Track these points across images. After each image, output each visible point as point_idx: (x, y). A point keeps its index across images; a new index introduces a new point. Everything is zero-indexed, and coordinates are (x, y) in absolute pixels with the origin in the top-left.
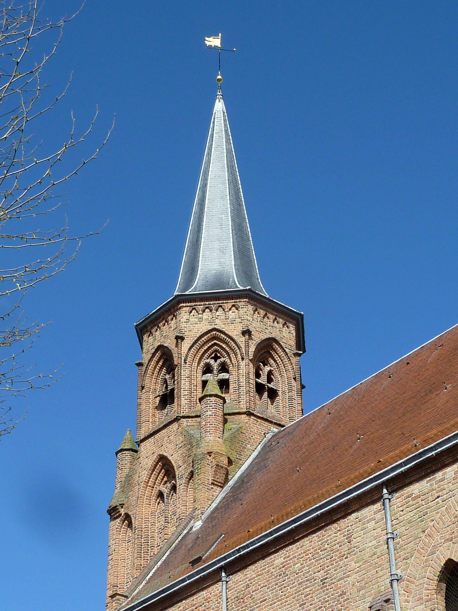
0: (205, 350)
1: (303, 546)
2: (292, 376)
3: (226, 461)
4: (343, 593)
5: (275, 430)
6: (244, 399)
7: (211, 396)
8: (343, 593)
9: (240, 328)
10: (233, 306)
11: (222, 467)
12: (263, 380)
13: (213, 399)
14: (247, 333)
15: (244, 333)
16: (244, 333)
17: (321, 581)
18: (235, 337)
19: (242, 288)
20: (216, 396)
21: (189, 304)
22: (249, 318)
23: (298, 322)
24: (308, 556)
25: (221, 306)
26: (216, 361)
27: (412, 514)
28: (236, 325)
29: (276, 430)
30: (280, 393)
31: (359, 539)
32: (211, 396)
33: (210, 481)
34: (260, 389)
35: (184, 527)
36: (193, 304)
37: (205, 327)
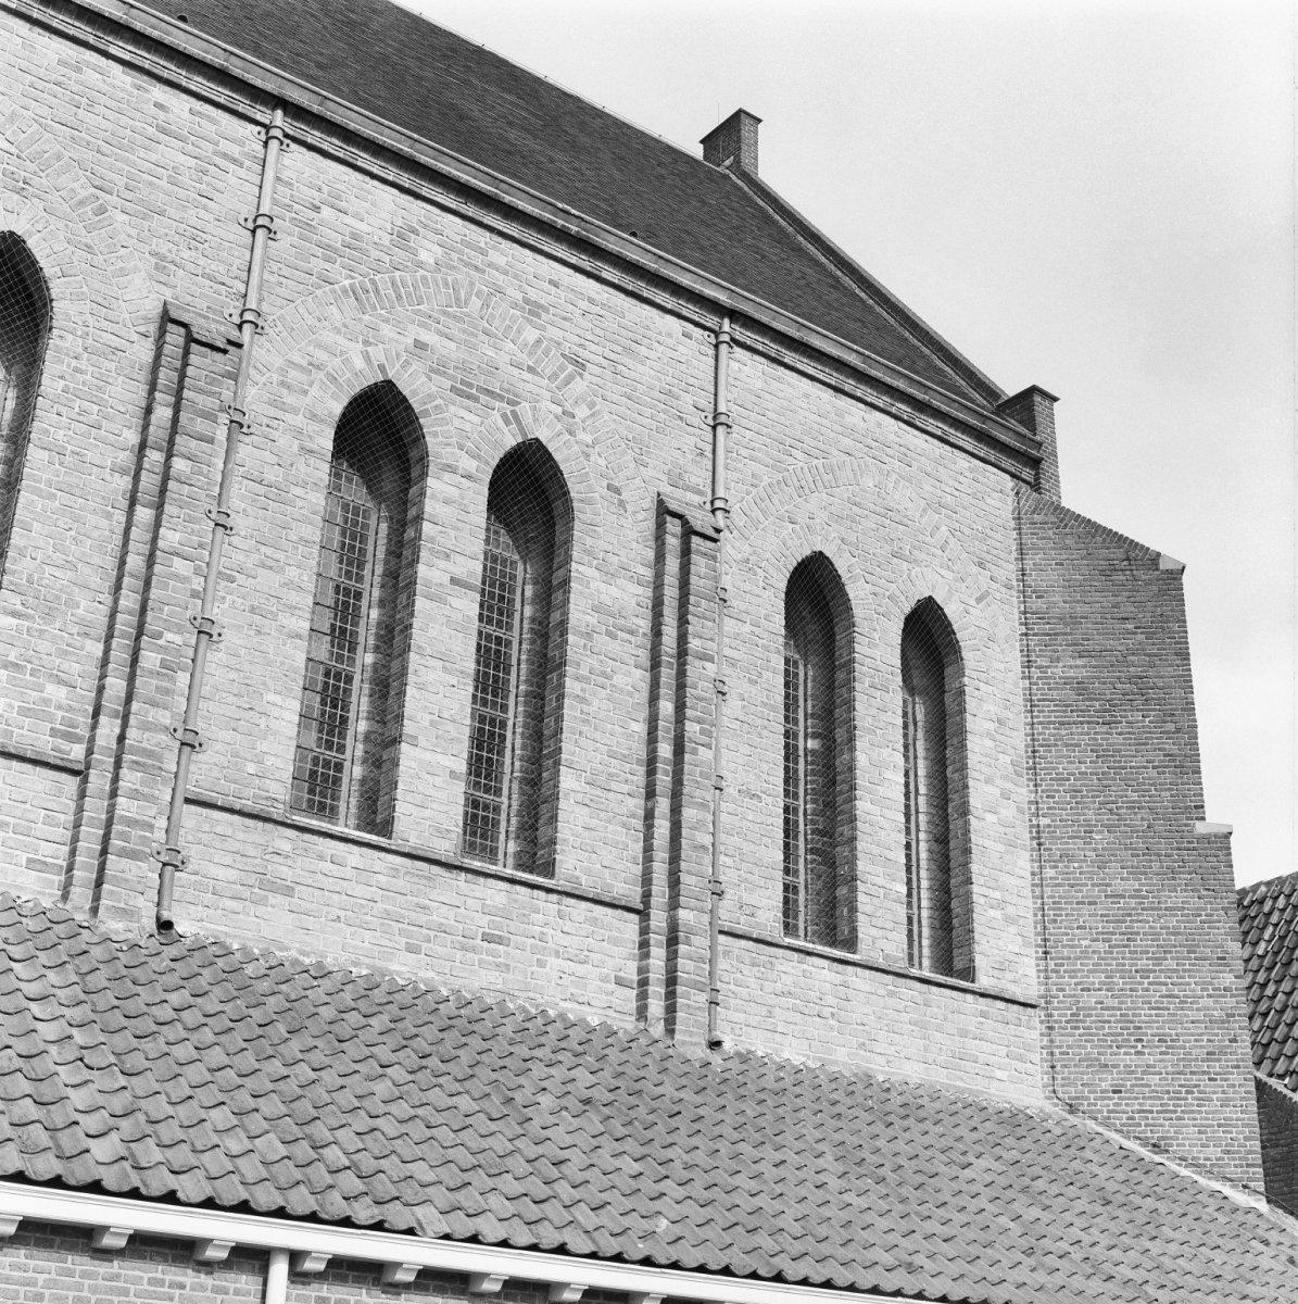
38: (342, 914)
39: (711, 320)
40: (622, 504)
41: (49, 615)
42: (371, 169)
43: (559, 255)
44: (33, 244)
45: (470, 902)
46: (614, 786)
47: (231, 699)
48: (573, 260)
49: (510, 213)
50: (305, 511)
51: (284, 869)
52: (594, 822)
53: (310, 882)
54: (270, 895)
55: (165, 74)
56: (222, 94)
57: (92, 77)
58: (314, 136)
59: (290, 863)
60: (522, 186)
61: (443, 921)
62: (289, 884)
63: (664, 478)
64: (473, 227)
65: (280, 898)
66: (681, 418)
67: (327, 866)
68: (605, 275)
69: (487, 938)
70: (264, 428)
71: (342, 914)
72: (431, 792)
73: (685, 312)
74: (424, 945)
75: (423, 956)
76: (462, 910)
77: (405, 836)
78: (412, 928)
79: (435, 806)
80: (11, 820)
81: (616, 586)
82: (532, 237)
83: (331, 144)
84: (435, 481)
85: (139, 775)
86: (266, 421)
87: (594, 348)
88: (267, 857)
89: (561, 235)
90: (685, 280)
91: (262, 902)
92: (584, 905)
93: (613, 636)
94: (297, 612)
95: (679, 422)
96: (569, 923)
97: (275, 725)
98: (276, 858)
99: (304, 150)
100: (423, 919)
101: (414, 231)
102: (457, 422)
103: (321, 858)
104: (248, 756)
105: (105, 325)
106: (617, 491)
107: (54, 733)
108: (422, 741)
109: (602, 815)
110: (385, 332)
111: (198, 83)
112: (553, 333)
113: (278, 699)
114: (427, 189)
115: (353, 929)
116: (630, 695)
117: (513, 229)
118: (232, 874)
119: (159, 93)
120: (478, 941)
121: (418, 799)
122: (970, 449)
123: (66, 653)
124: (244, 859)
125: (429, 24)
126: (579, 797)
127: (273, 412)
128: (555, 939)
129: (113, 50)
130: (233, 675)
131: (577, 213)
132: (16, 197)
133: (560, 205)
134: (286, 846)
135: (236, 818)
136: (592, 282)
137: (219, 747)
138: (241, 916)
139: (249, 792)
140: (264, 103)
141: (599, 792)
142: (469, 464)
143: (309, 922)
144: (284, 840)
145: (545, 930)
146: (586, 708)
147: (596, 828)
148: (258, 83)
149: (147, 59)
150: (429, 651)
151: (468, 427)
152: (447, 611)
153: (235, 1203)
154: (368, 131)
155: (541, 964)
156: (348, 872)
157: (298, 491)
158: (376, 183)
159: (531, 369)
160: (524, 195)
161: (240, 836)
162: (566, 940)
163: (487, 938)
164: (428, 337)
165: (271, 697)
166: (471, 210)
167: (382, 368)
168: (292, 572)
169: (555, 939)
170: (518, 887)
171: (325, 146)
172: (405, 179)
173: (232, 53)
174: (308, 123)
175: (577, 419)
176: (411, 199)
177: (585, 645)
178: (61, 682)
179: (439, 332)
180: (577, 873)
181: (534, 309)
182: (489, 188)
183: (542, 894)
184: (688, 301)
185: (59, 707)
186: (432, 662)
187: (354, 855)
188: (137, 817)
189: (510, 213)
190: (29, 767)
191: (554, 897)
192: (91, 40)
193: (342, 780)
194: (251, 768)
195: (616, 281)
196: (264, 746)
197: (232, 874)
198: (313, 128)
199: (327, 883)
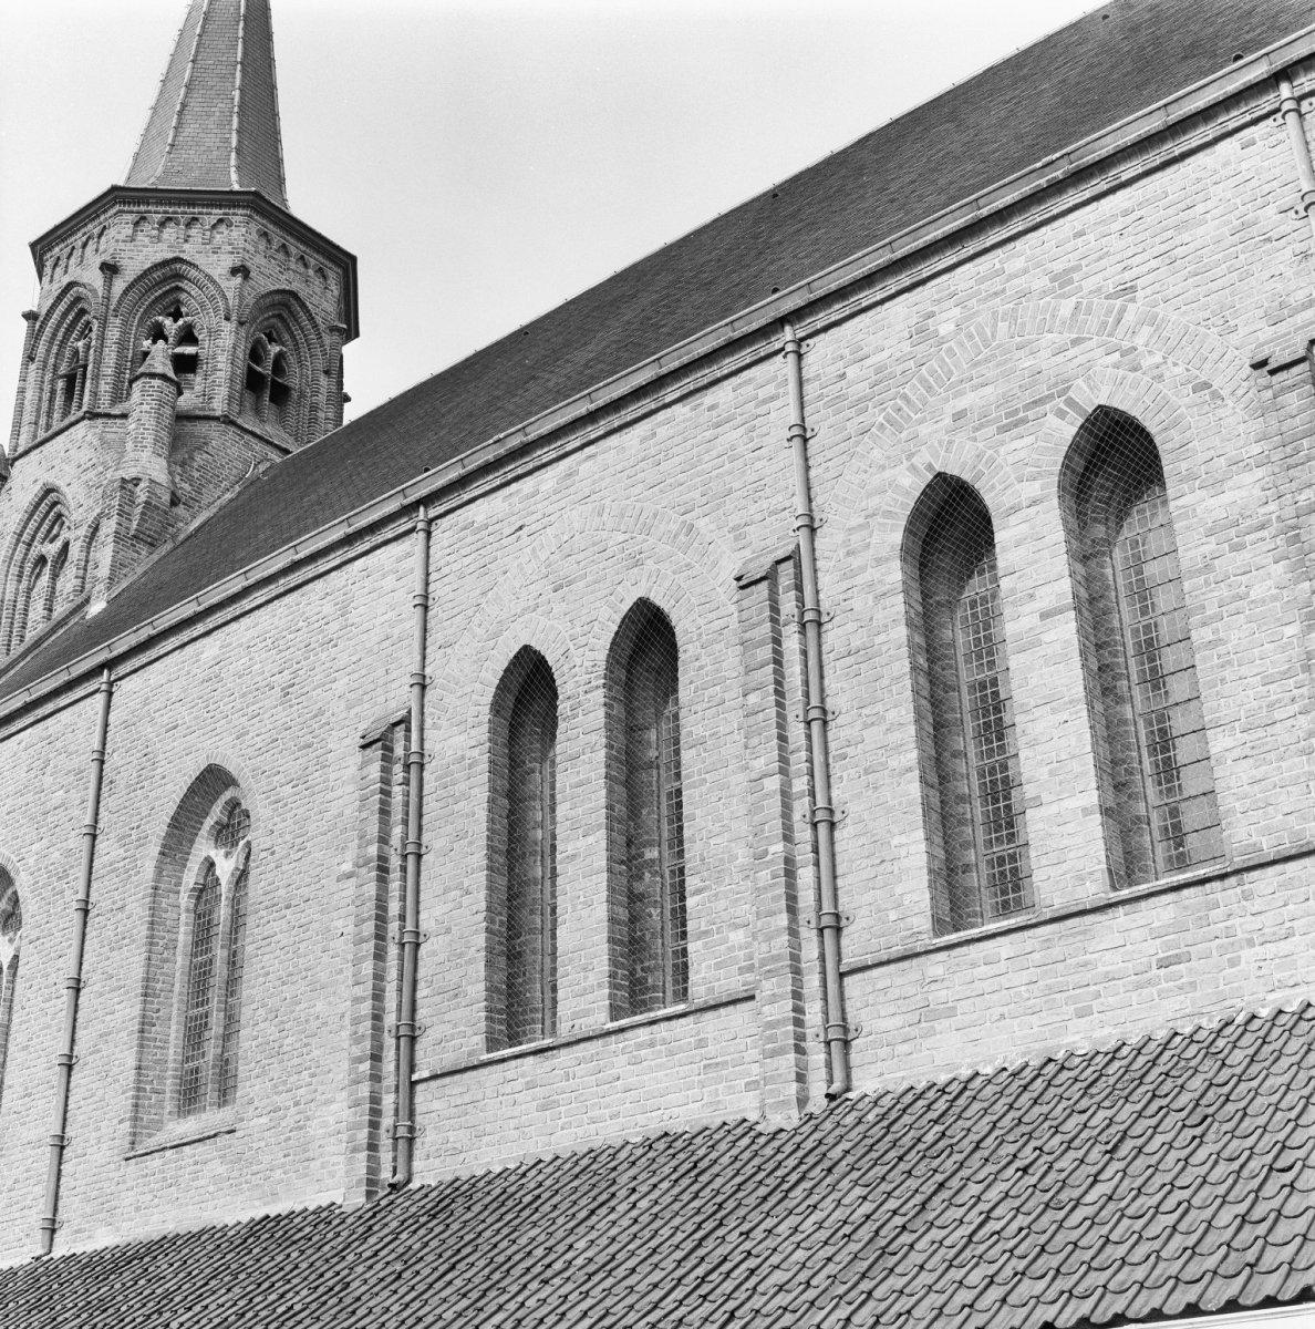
0: (156, 298)
1: (257, 624)
2: (320, 367)
3: (166, 498)
4: (321, 712)
5: (277, 458)
6: (222, 393)
7: (153, 376)
8: (321, 712)
9: (229, 261)
10: (221, 221)
11: (158, 508)
12: (266, 369)
13: (156, 382)
14: (241, 271)
15: (234, 271)
16: (234, 271)
17: (282, 690)
18: (216, 278)
19: (236, 187)
20: (163, 377)
21: (136, 209)
22: (249, 247)
23: (346, 271)
24: (264, 644)
25: (197, 219)
26: (175, 321)
27: (467, 561)
28: (223, 257)
29: (278, 460)
30: (295, 395)
31: (362, 610)
32: (153, 376)
33: (132, 532)
34: (253, 382)
35: (382, 791)
36: (142, 208)
37: (162, 253)
38: (1005, 1010)
39: (1266, 103)
40: (1216, 396)
41: (719, 881)
42: (874, 300)
43: (1070, 204)
44: (1116, 404)
45: (1134, 934)
46: (1277, 715)
47: (865, 862)
48: (1087, 195)
49: (1001, 216)
50: (892, 652)
51: (944, 992)
52: (1258, 774)
53: (968, 994)
54: (936, 1024)
55: (705, 381)
56: (745, 356)
57: (662, 432)
58: (822, 318)
59: (946, 984)
60: (841, 263)
61: (1109, 968)
62: (950, 1004)
63: (1262, 324)
64: (983, 258)
65: (945, 1023)
66: (1269, 240)
67: (983, 970)
68: (1124, 177)
69: (1164, 964)
70: (843, 604)
71: (1005, 1010)
72: (1065, 842)
73: (1231, 125)
74: (1094, 1003)
75: (1096, 1015)
76: (1128, 947)
77: (1048, 902)
78: (1078, 991)
79: (1071, 855)
80: (729, 1058)
81: (1230, 489)
82: (1036, 214)
83: (836, 311)
84: (1003, 532)
85: (774, 980)
86: (842, 597)
87: (1138, 259)
88: (926, 989)
89: (1057, 188)
90: (1200, 102)
91: (932, 1033)
92: (1270, 871)
93: (1237, 548)
94: (901, 749)
95: (1269, 245)
96: (1259, 900)
97: (905, 863)
98: (934, 986)
99: (822, 336)
100: (1087, 976)
101: (931, 315)
102: (1011, 459)
103: (974, 965)
104: (889, 906)
105: (712, 616)
106: (1207, 385)
107: (741, 971)
108: (1045, 797)
109: (1272, 756)
110: (925, 432)
111: (729, 363)
112: (1089, 285)
113: (903, 839)
114: (925, 269)
115: (1018, 1020)
116: (1275, 598)
117: (1017, 224)
118: (898, 1021)
119: (709, 398)
120: (1154, 971)
121: (1053, 857)
122: (554, 455)
123: (736, 900)
124: (907, 1001)
125: (610, 280)
126: (1237, 753)
127: (845, 585)
128: (1243, 925)
129: (668, 399)
130: (863, 840)
131: (1058, 155)
132: (636, 569)
133: (1039, 165)
134: (938, 971)
135: (892, 967)
136: (1120, 194)
137: (864, 911)
138: (915, 1055)
139: (894, 939)
140: (775, 332)
141: (1260, 733)
142: (1032, 489)
143: (974, 1033)
144: (935, 966)
145: (1228, 923)
146: (1222, 649)
147: (729, 926)
148: (755, 326)
149: (689, 383)
150: (1033, 703)
151: (1022, 454)
152: (1040, 651)
153: (1181, 1309)
154: (441, 482)
155: (1233, 963)
156: (1002, 967)
157: (882, 637)
158: (887, 305)
159: (1075, 342)
160: (1034, 174)
161: (899, 981)
162: (1257, 923)
163: (1164, 964)
164: (962, 403)
165: (895, 842)
166: (972, 247)
167: (930, 467)
168: (892, 715)
169: (1243, 925)
170: (1186, 892)
171: (834, 318)
172: (905, 279)
173: (1165, 106)
174: (811, 314)
175: (1140, 349)
176: (920, 288)
177: (1206, 581)
178: (736, 927)
179: (975, 388)
180: (1254, 839)
181: (1062, 279)
182: (963, 220)
183: (1216, 885)
184: (1228, 110)
185: (740, 948)
186: (1037, 712)
187: (1003, 946)
188: (779, 1017)
189: (1001, 216)
190: (731, 1008)
191: (1233, 880)
192: (653, 406)
193: (980, 875)
194: (893, 916)
195: (1140, 171)
196: (899, 890)
197: (898, 1021)
198: (817, 313)
199: (986, 986)
